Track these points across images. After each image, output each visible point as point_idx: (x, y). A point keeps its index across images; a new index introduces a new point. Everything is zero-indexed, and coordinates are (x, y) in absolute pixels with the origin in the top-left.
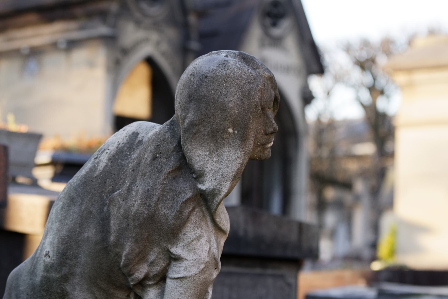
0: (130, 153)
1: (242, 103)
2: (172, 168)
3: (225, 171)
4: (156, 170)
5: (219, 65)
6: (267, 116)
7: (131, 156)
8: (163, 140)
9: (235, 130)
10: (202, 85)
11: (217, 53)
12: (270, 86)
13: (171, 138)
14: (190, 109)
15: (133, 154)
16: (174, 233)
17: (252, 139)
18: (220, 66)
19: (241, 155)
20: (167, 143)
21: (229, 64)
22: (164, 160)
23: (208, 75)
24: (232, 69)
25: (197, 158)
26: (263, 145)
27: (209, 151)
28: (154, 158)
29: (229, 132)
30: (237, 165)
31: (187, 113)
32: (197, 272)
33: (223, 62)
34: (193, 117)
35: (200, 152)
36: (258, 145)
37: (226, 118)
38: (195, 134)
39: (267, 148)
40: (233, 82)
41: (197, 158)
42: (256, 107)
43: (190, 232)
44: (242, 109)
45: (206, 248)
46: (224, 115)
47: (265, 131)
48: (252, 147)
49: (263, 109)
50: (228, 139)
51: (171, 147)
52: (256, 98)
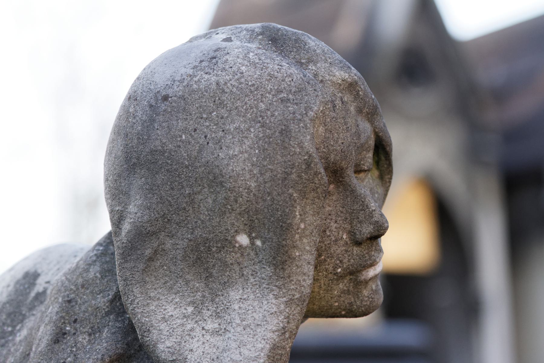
0: (14, 327)
1: (264, 159)
6: (353, 191)
7: (15, 335)
8: (83, 286)
9: (256, 238)
10: (154, 120)
12: (352, 109)
14: (132, 193)
15: (19, 330)
17: (310, 258)
18: (204, 64)
19: (278, 306)
20: (92, 292)
21: (227, 57)
22: (83, 339)
23: (170, 92)
25: (163, 326)
26: (351, 273)
27: (193, 303)
28: (59, 337)
29: (241, 246)
30: (269, 335)
33: (212, 54)
34: (139, 214)
35: (170, 310)
37: (225, 205)
38: (151, 259)
39: (366, 282)
40: (239, 103)
41: (163, 326)
42: (308, 165)
44: (268, 174)
46: (220, 197)
47: (352, 233)
49: (336, 174)
50: (239, 264)
51: (102, 301)
52: (307, 141)
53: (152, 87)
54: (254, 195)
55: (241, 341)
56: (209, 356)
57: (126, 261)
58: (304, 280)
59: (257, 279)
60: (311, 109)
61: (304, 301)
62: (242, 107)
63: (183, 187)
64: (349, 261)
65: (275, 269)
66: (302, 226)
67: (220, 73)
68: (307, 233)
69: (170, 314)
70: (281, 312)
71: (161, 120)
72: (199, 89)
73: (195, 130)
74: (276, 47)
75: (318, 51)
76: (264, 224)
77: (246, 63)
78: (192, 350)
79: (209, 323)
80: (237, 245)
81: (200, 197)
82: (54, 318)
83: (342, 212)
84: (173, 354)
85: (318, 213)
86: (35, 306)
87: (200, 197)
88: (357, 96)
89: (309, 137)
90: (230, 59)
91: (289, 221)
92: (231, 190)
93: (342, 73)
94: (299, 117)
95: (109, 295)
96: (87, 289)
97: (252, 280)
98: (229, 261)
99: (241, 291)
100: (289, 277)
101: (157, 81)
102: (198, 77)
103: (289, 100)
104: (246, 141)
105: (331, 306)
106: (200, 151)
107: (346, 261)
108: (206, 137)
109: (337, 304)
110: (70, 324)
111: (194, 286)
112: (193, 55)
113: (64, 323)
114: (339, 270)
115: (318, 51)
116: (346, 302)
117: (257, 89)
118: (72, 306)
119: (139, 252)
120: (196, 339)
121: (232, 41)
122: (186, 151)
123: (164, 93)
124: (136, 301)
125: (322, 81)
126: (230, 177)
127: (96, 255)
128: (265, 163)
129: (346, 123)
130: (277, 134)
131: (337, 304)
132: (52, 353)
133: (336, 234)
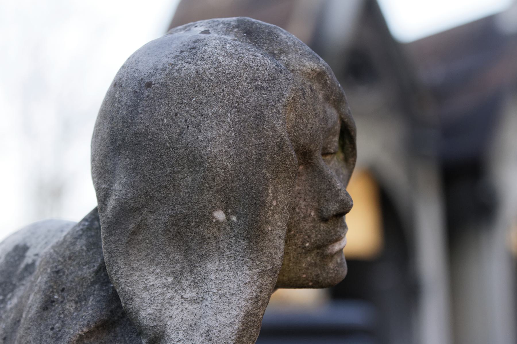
1: (240, 142)
2: (88, 325)
3: (213, 323)
4: (51, 333)
5: (182, 52)
6: (321, 172)
8: (70, 258)
9: (232, 214)
10: (138, 106)
11: (184, 29)
12: (320, 96)
13: (88, 250)
14: (117, 172)
15: (10, 299)
17: (281, 232)
18: (184, 54)
19: (252, 277)
20: (78, 263)
21: (206, 48)
22: (70, 306)
23: (153, 79)
24: (213, 58)
25: (145, 295)
26: (318, 247)
27: (172, 273)
28: (48, 304)
29: (218, 221)
30: (243, 303)
31: (111, 183)
33: (192, 45)
35: (152, 280)
36: (304, 248)
37: (203, 184)
38: (134, 233)
40: (216, 90)
41: (145, 295)
42: (281, 148)
44: (243, 156)
46: (199, 176)
47: (319, 211)
48: (280, 255)
49: (305, 156)
50: (216, 238)
51: (87, 272)
52: (279, 125)
53: (136, 75)
55: (217, 309)
56: (187, 323)
57: (111, 235)
58: (276, 253)
61: (276, 272)
62: (220, 93)
64: (316, 236)
65: (249, 243)
66: (274, 203)
67: (199, 62)
68: (279, 209)
69: (151, 284)
72: (180, 77)
73: (176, 115)
74: (250, 39)
75: (289, 43)
76: (239, 201)
77: (223, 53)
78: (171, 317)
79: (187, 292)
80: (214, 220)
81: (181, 176)
83: (310, 191)
84: (154, 320)
85: (289, 192)
87: (181, 176)
88: (325, 85)
89: (281, 122)
91: (262, 199)
92: (209, 170)
93: (311, 63)
94: (272, 103)
95: (94, 266)
96: (74, 260)
97: (228, 253)
98: (207, 234)
99: (217, 263)
100: (262, 250)
101: (141, 70)
102: (179, 66)
103: (263, 87)
104: (223, 125)
107: (313, 236)
108: (186, 121)
109: (304, 276)
110: (58, 292)
111: (174, 258)
112: (174, 46)
113: (53, 292)
114: (307, 244)
115: (289, 43)
116: (314, 273)
117: (233, 77)
118: (60, 277)
119: (123, 226)
120: (175, 307)
122: (168, 134)
123: (147, 81)
124: (120, 271)
125: (293, 71)
126: (208, 158)
128: (241, 145)
129: (315, 110)
130: (252, 118)
131: (304, 276)
133: (305, 211)
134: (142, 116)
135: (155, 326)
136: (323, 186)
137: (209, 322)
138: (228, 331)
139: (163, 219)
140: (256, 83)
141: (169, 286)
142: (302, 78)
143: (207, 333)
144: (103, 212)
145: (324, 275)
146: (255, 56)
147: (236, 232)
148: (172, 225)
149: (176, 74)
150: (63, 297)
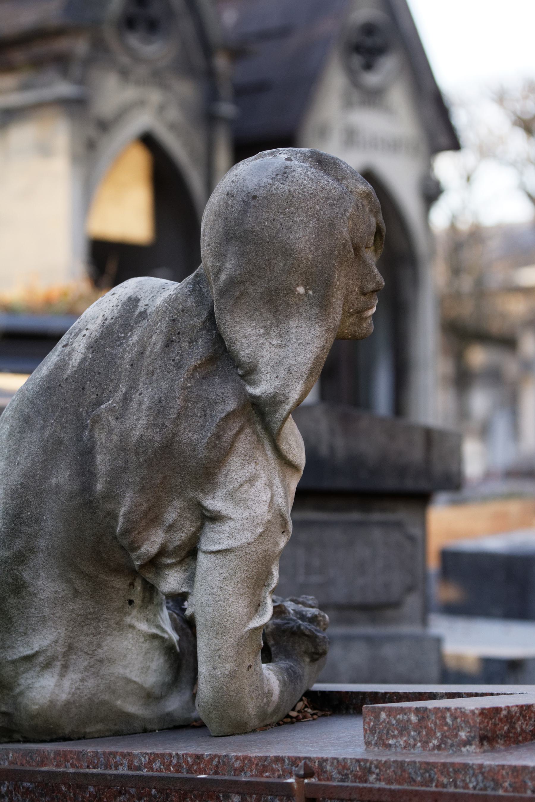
1: (318, 241)
3: (294, 362)
4: (173, 363)
6: (364, 261)
8: (183, 311)
9: (309, 289)
10: (247, 211)
12: (367, 209)
14: (229, 255)
15: (130, 336)
16: (208, 474)
17: (340, 303)
18: (279, 177)
19: (321, 333)
20: (190, 315)
21: (294, 173)
22: (185, 345)
23: (257, 194)
25: (244, 340)
27: (264, 327)
28: (169, 343)
29: (299, 294)
30: (315, 350)
32: (251, 540)
33: (283, 170)
34: (233, 270)
35: (249, 330)
38: (238, 298)
39: (366, 318)
40: (303, 205)
41: (244, 340)
42: (345, 247)
43: (236, 470)
44: (320, 251)
45: (266, 497)
46: (289, 263)
47: (361, 288)
48: (339, 318)
49: (357, 249)
51: (198, 322)
53: (245, 189)
54: (311, 263)
55: (296, 353)
56: (274, 361)
57: (222, 298)
58: (337, 317)
59: (308, 314)
60: (347, 211)
61: (336, 330)
62: (305, 207)
63: (264, 255)
64: (358, 305)
65: (320, 309)
66: (338, 283)
67: (290, 184)
68: (340, 287)
69: (249, 333)
70: (322, 336)
71: (252, 211)
72: (277, 194)
73: (274, 220)
74: (322, 167)
75: (348, 172)
76: (315, 281)
77: (306, 178)
78: (262, 357)
79: (274, 340)
80: (297, 293)
81: (275, 262)
82: (164, 330)
83: (356, 274)
84: (250, 358)
85: (347, 276)
86: (140, 321)
87: (275, 262)
88: (370, 202)
89: (346, 229)
90: (296, 175)
91: (331, 281)
92: (297, 259)
93: (363, 187)
94: (340, 216)
95: (202, 318)
96: (187, 313)
97: (305, 315)
98: (291, 302)
99: (297, 322)
100: (329, 315)
101: (248, 185)
102: (276, 186)
103: (334, 204)
104: (307, 229)
105: (343, 332)
106: (277, 233)
107: (355, 305)
108: (281, 224)
109: (346, 331)
110: (175, 335)
111: (266, 316)
112: (270, 169)
113: (171, 334)
114: (351, 310)
115: (348, 172)
116: (353, 330)
117: (314, 196)
118: (176, 324)
119: (231, 293)
120: (265, 350)
121: (291, 160)
122: (268, 233)
123: (253, 194)
124: (227, 324)
125: (351, 192)
126: (297, 251)
127: (189, 291)
128: (319, 244)
129: (364, 219)
130: (327, 226)
131: (346, 331)
132: (165, 353)
133: (352, 287)
134: (250, 219)
135: (250, 362)
136: (365, 271)
137: (290, 362)
138: (304, 368)
139: (260, 290)
140: (330, 201)
141: (261, 335)
142: (356, 196)
143: (289, 369)
144: (216, 282)
145: (360, 331)
146: (327, 181)
147: (311, 301)
148: (267, 294)
149: (274, 191)
150: (179, 339)
